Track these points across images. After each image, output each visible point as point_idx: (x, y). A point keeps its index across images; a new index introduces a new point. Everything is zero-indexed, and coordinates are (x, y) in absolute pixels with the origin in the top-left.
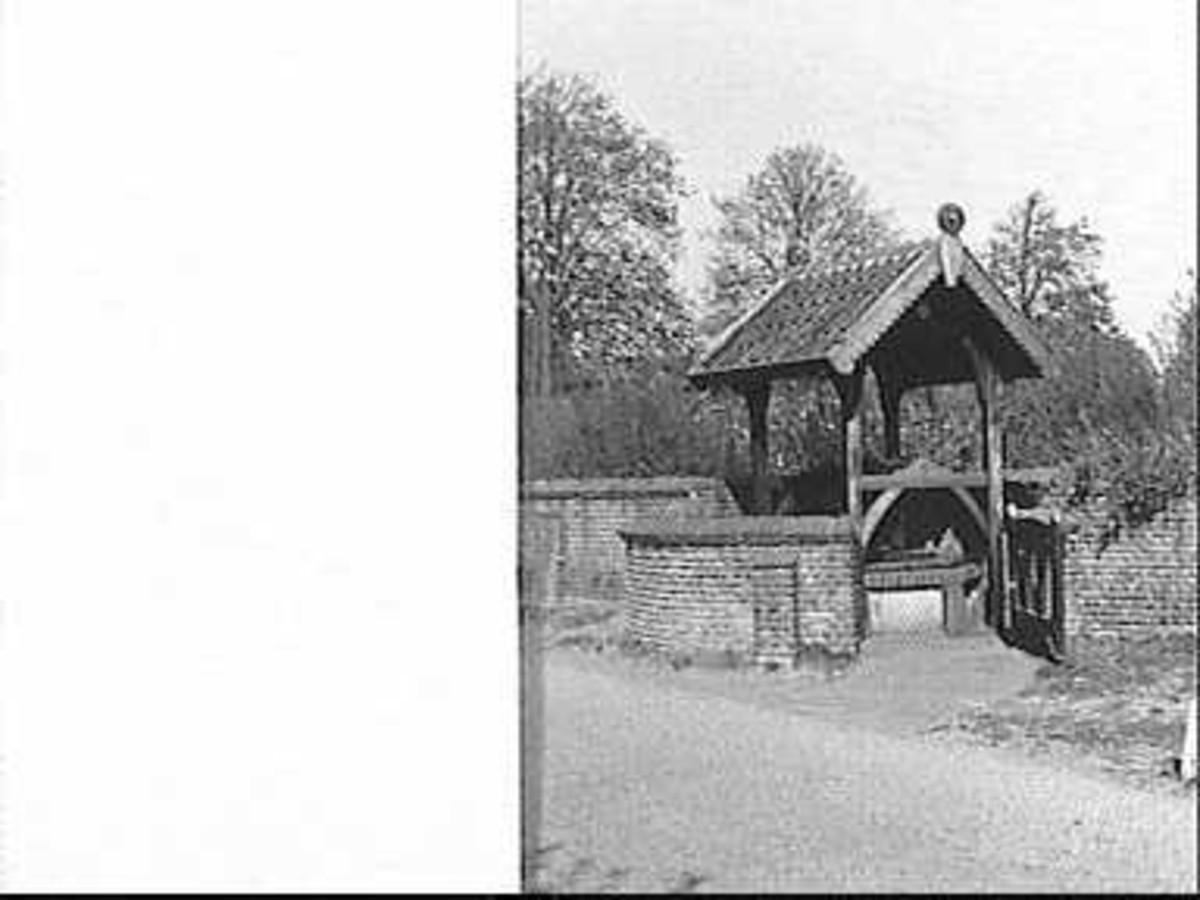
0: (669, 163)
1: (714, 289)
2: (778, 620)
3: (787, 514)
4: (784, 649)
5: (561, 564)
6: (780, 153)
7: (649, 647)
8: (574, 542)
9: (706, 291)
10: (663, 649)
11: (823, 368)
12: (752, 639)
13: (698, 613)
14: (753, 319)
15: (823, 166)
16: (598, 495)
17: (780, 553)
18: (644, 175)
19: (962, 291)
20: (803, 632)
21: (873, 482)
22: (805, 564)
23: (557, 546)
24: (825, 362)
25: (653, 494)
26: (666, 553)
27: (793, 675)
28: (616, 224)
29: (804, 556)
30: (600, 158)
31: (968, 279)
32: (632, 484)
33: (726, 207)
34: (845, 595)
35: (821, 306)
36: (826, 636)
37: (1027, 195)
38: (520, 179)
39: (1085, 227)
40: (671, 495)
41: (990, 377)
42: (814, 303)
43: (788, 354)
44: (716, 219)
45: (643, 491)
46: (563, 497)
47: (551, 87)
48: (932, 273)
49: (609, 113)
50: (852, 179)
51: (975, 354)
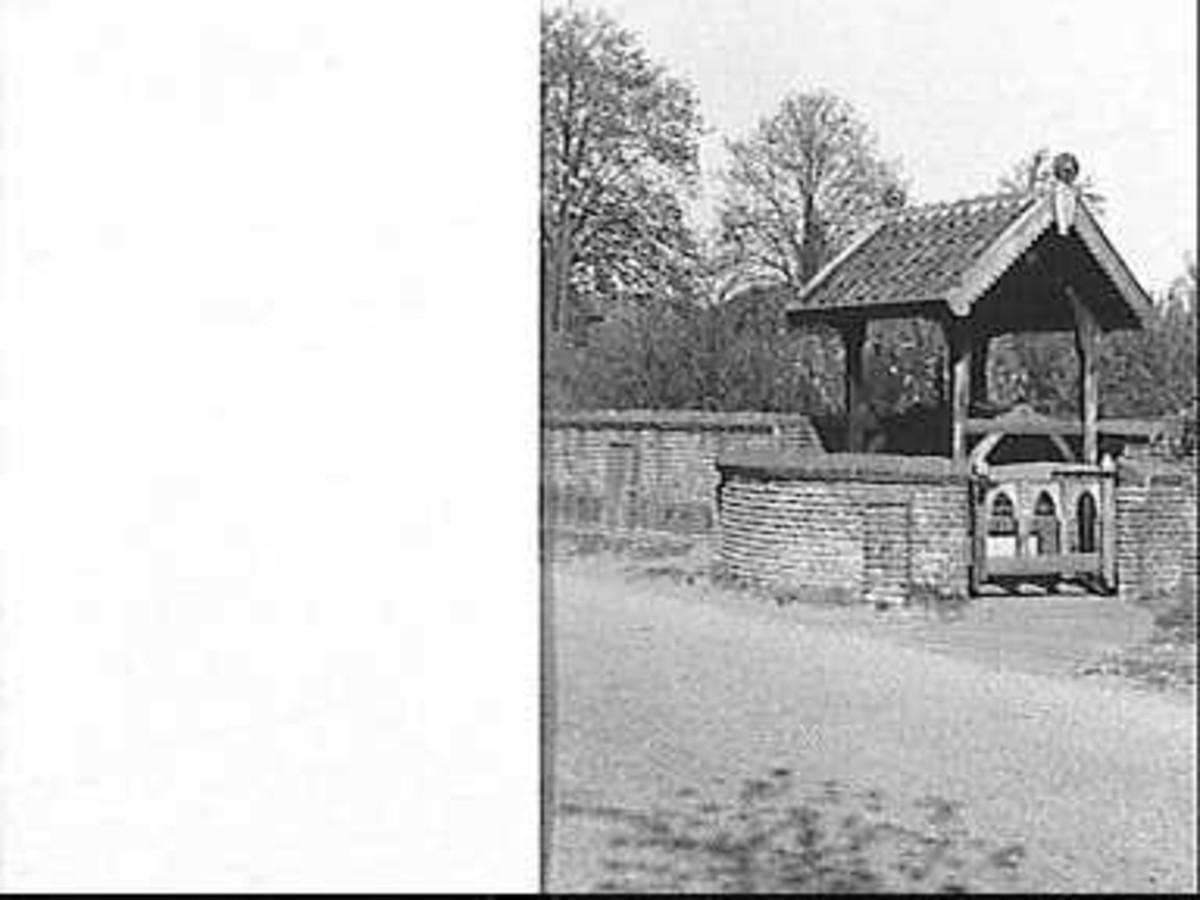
0: (688, 102)
1: (722, 230)
2: (891, 558)
3: (879, 451)
4: (895, 588)
5: (633, 494)
6: (794, 99)
7: (749, 581)
8: (648, 470)
9: (715, 231)
10: (764, 583)
11: (937, 310)
12: (860, 577)
13: (805, 548)
14: (848, 259)
15: (838, 112)
16: (674, 426)
17: (896, 492)
18: (665, 113)
19: (1073, 239)
20: (914, 570)
21: (976, 424)
22: (920, 504)
23: (629, 474)
24: (943, 303)
25: (733, 429)
26: (771, 486)
27: (905, 614)
28: (635, 161)
29: (919, 495)
30: (622, 92)
31: (1079, 229)
32: (711, 418)
33: (737, 149)
34: (958, 537)
35: (927, 249)
36: (937, 576)
37: (1034, 150)
38: (543, 111)
39: (1089, 186)
40: (752, 429)
41: (1090, 328)
42: (918, 245)
43: (894, 295)
44: (726, 161)
45: (725, 424)
46: (639, 427)
47: (577, 22)
48: (1047, 218)
49: (629, 50)
50: (864, 128)
51: (1076, 301)
